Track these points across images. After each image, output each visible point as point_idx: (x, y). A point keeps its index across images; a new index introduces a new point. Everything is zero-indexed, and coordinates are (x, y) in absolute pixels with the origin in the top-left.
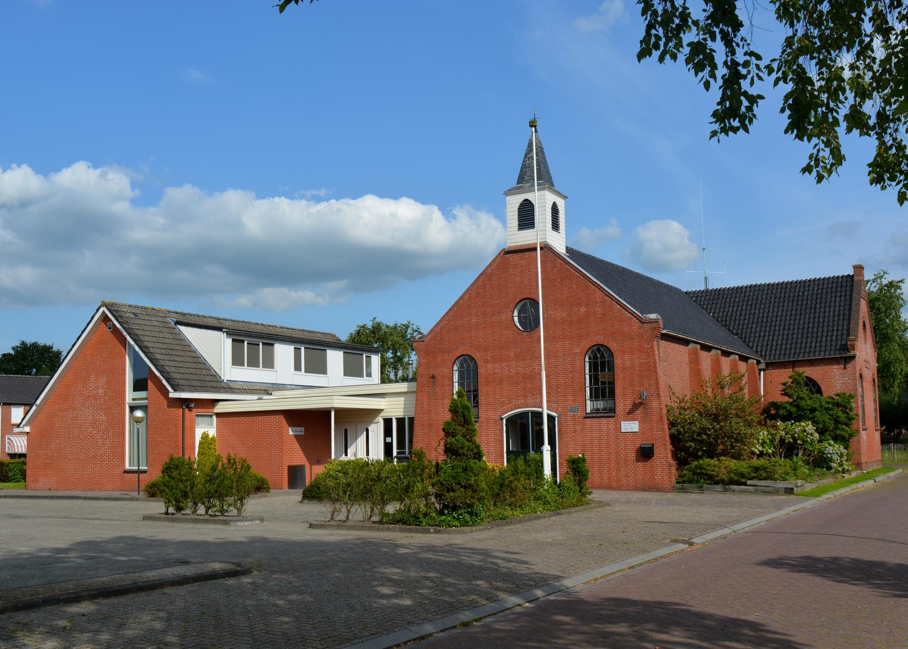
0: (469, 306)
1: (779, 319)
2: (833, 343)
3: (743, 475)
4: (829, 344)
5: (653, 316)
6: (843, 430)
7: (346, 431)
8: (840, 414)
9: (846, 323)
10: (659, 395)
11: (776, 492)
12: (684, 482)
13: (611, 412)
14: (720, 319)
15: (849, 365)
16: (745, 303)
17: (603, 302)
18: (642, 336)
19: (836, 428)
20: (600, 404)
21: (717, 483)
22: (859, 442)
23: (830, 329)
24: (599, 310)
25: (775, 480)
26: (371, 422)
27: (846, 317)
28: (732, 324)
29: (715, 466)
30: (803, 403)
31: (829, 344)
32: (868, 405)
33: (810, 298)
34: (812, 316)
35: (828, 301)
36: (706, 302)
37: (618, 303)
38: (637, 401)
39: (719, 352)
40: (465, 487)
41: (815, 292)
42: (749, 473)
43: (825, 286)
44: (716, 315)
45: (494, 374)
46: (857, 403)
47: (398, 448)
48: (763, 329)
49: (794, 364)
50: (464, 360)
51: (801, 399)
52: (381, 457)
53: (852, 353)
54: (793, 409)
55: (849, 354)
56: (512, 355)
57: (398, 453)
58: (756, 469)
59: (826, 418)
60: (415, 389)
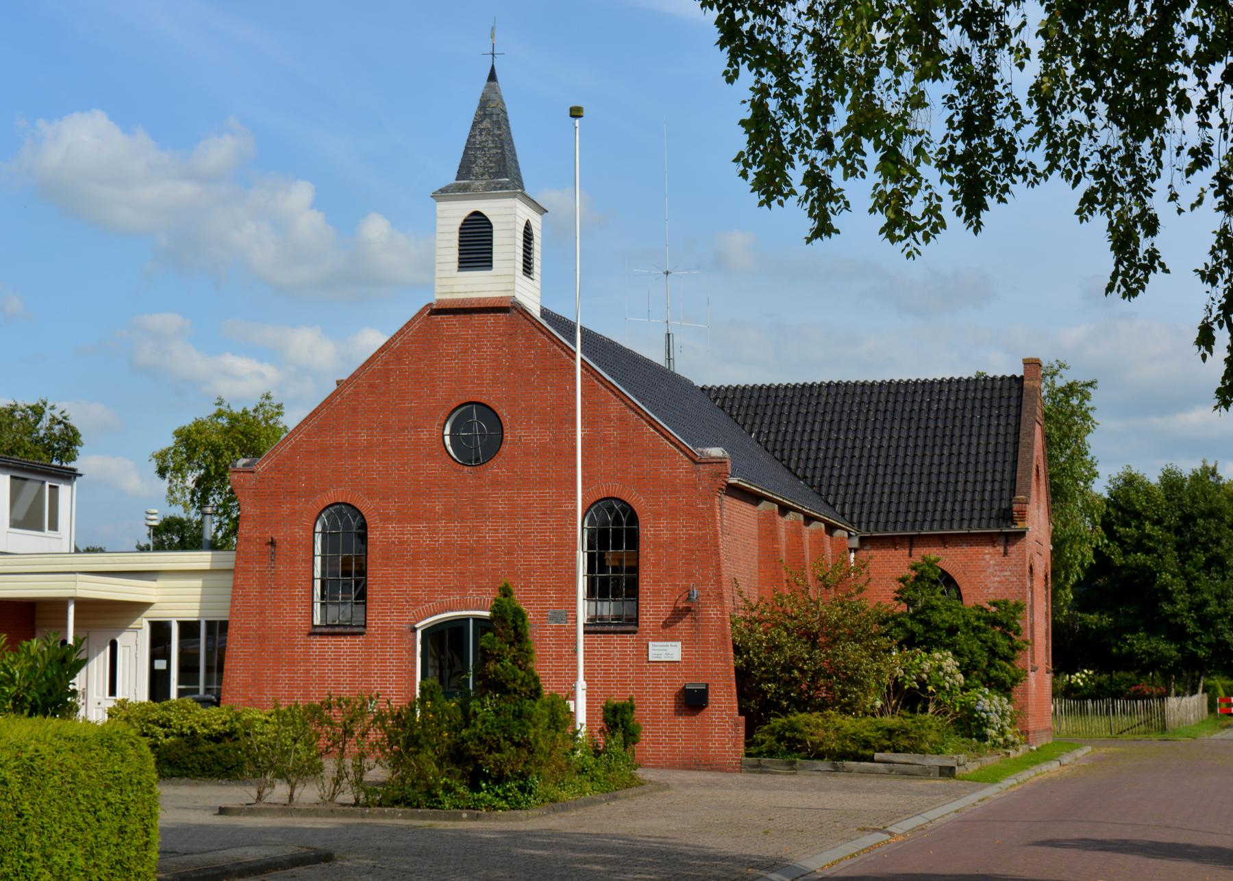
0: (354, 409)
1: (883, 453)
2: (986, 506)
3: (867, 744)
4: (977, 506)
5: (716, 452)
6: (1003, 669)
7: (114, 645)
8: (999, 640)
9: (1008, 468)
10: (720, 597)
11: (925, 773)
12: (760, 754)
13: (629, 623)
14: (770, 447)
15: (1012, 549)
16: (819, 419)
17: (622, 419)
18: (695, 487)
19: (990, 665)
20: (607, 609)
21: (820, 756)
22: (1025, 693)
23: (980, 478)
24: (613, 433)
25: (923, 752)
26: (123, 628)
27: (1009, 458)
28: (795, 458)
29: (817, 726)
30: (936, 617)
31: (977, 506)
32: (1038, 626)
33: (941, 416)
34: (946, 452)
35: (976, 424)
36: (742, 412)
37: (652, 423)
38: (682, 605)
39: (801, 517)
40: (518, 745)
41: (951, 406)
42: (877, 739)
43: (971, 395)
44: (763, 439)
45: (401, 543)
46: (1024, 619)
47: (180, 683)
48: (854, 472)
49: (912, 541)
50: (339, 512)
51: (933, 608)
52: (144, 696)
53: (1019, 526)
54: (918, 628)
55: (1014, 528)
56: (439, 508)
57: (181, 693)
58: (891, 732)
59: (976, 645)
60: (231, 566)
